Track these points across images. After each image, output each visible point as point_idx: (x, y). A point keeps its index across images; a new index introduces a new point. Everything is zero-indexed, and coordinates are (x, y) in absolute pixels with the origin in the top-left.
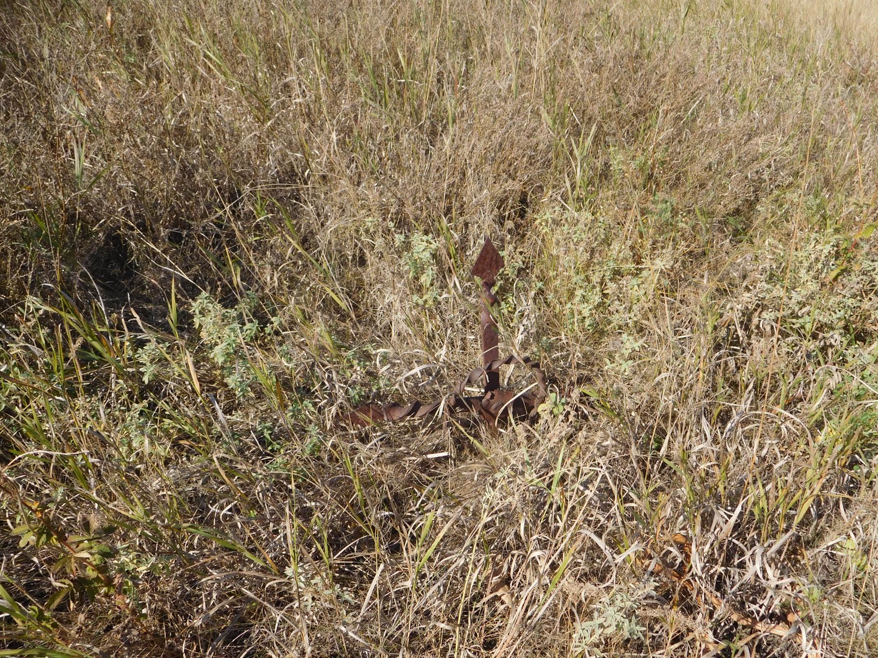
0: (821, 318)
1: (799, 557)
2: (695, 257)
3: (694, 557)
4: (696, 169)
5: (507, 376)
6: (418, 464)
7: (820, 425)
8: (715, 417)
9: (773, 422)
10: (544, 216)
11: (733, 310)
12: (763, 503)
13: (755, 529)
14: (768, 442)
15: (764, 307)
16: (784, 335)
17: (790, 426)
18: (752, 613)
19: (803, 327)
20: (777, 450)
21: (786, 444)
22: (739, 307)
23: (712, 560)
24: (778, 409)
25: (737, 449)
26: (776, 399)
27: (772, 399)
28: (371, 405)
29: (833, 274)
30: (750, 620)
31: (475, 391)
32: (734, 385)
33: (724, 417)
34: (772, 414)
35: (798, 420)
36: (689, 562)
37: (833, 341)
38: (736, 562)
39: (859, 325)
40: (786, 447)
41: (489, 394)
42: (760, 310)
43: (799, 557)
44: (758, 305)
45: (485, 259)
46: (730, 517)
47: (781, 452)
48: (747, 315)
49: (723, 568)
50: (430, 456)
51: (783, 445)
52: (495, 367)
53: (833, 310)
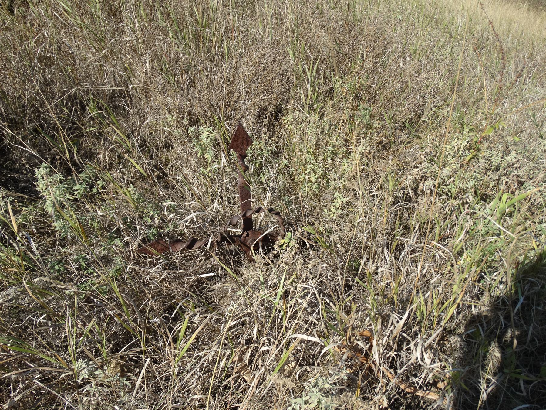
0: (461, 185)
1: (445, 342)
2: (384, 146)
3: (375, 349)
4: (386, 93)
5: (260, 221)
6: (193, 281)
7: (460, 253)
8: (394, 248)
9: (430, 251)
10: (288, 119)
11: (408, 181)
12: (423, 308)
13: (417, 325)
14: (427, 264)
15: (426, 178)
16: (439, 195)
17: (441, 254)
18: (414, 383)
19: (449, 191)
20: (433, 271)
21: (438, 266)
22: (411, 177)
23: (388, 348)
24: (434, 243)
25: (407, 269)
26: (433, 236)
27: (430, 236)
28: (162, 242)
29: (468, 158)
30: (412, 388)
31: (239, 231)
32: (407, 228)
33: (400, 248)
34: (430, 246)
35: (447, 250)
36: (371, 352)
37: (468, 200)
38: (405, 348)
39: (483, 191)
40: (438, 268)
41: (245, 233)
42: (423, 179)
43: (445, 342)
44: (422, 177)
45: (238, 139)
46: (401, 319)
47: (435, 271)
48: (416, 183)
49: (396, 353)
50: (202, 276)
51: (437, 267)
52: (248, 214)
53: (467, 181)
